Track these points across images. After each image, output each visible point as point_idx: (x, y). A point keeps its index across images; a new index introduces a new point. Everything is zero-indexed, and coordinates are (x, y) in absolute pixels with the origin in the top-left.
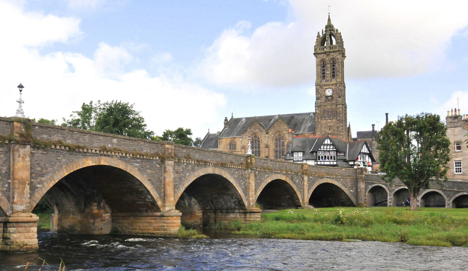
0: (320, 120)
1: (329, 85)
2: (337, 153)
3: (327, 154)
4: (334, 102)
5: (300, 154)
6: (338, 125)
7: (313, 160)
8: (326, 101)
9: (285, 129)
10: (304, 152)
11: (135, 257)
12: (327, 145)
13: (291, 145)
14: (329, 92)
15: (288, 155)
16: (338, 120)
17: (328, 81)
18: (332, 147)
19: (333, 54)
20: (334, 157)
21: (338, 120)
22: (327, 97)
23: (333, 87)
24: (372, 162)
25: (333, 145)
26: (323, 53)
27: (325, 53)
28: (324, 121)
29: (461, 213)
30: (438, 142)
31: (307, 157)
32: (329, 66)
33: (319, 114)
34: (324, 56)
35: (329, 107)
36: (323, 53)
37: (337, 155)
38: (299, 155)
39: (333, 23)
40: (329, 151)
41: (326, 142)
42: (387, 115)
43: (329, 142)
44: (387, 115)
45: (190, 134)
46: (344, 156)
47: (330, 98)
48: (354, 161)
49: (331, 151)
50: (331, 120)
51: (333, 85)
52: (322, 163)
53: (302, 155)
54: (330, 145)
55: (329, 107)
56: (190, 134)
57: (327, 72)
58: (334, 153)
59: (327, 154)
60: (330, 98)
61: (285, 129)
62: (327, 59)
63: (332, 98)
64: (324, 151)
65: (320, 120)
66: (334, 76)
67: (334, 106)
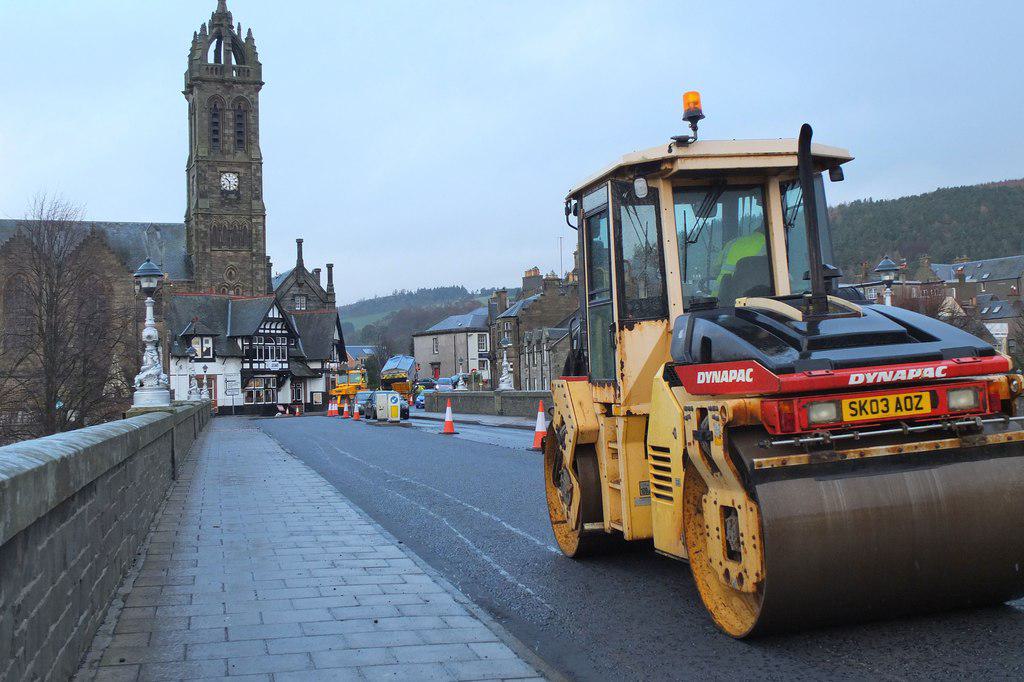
0: (208, 250)
1: (230, 164)
4: (244, 207)
5: (207, 342)
8: (223, 204)
11: (198, 182)
12: (273, 320)
14: (230, 181)
16: (253, 255)
17: (229, 153)
18: (279, 327)
19: (240, 87)
21: (253, 255)
22: (225, 193)
23: (242, 170)
26: (216, 81)
27: (222, 82)
29: (474, 431)
31: (225, 351)
32: (230, 115)
34: (219, 90)
35: (230, 218)
36: (216, 81)
39: (230, 7)
41: (270, 316)
42: (300, 242)
43: (276, 316)
44: (300, 242)
45: (837, 176)
47: (233, 196)
49: (280, 335)
50: (235, 251)
51: (240, 165)
52: (262, 366)
53: (210, 345)
54: (277, 321)
55: (230, 218)
56: (837, 176)
57: (226, 131)
60: (233, 196)
62: (226, 97)
63: (239, 198)
66: (240, 141)
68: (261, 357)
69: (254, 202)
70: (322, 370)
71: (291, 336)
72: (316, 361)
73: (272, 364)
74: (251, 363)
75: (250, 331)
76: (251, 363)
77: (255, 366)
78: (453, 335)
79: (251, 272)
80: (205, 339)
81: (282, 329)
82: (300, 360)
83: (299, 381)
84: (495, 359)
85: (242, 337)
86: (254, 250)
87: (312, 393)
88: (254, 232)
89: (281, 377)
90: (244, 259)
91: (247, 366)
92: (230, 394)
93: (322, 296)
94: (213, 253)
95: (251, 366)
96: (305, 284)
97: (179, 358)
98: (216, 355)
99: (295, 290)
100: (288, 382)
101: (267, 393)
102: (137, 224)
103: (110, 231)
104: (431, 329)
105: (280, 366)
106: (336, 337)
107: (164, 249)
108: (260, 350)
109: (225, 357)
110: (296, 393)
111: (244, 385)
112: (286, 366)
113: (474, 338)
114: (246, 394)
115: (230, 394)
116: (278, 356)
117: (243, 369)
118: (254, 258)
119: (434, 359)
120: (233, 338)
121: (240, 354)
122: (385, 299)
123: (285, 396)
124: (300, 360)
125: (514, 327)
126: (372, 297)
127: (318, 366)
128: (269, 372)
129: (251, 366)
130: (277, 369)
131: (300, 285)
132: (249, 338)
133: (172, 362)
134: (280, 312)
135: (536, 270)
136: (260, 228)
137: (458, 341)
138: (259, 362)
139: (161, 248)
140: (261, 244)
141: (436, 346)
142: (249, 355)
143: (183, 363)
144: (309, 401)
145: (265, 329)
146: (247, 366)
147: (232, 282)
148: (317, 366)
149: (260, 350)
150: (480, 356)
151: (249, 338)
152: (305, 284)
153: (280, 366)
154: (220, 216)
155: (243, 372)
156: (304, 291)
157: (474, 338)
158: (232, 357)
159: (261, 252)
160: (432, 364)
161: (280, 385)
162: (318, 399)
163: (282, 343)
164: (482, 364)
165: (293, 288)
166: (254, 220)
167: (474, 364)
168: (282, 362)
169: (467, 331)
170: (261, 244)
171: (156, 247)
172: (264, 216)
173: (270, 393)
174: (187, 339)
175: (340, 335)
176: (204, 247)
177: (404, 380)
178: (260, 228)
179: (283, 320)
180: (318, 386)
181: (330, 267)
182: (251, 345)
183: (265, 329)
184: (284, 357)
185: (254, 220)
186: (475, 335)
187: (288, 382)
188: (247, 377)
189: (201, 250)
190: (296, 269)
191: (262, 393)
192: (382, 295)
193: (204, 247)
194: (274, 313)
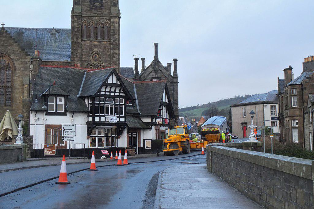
0: (80, 40)
2: (125, 102)
3: (110, 104)
4: (105, 12)
5: (60, 100)
6: (112, 52)
7: (85, 112)
8: (91, 9)
9: (13, 52)
10: (66, 97)
12: (112, 85)
13: (38, 81)
15: (36, 101)
16: (111, 44)
18: (118, 90)
20: (121, 109)
21: (111, 44)
24: (170, 118)
25: (120, 85)
28: (87, 43)
30: (84, 103)
31: (74, 107)
33: (78, 29)
37: (125, 105)
38: (59, 103)
40: (114, 97)
41: (110, 81)
42: (156, 45)
43: (115, 82)
44: (156, 45)
46: (133, 106)
48: (152, 117)
50: (99, 42)
52: (103, 119)
53: (63, 103)
54: (116, 86)
55: (96, 19)
58: (121, 101)
59: (110, 104)
61: (13, 52)
64: (105, 96)
65: (80, 40)
67: (105, 20)
68: (102, 113)
69: (113, 8)
70: (152, 124)
71: (128, 98)
72: (147, 117)
73: (113, 119)
74: (94, 117)
75: (92, 93)
76: (94, 117)
77: (97, 119)
78: (254, 106)
79: (110, 55)
80: (58, 98)
81: (120, 93)
82: (136, 116)
83: (134, 132)
84: (283, 118)
85: (88, 97)
86: (112, 41)
87: (144, 140)
88: (112, 28)
89: (119, 128)
90: (105, 47)
91: (91, 119)
92: (79, 139)
93: (170, 78)
94: (83, 43)
95: (93, 119)
96: (159, 71)
97: (36, 111)
98: (70, 110)
99: (153, 75)
100: (125, 132)
101: (107, 140)
102: (46, 29)
103: (26, 33)
104: (242, 103)
105: (118, 120)
106: (165, 99)
107: (57, 44)
108: (102, 108)
109: (73, 112)
110: (132, 141)
111: (89, 133)
112: (123, 120)
113: (268, 108)
114: (91, 140)
115: (79, 139)
116: (112, 113)
117: (88, 121)
118: (112, 46)
119: (243, 120)
120: (82, 98)
121: (86, 110)
122: (231, 99)
123: (123, 142)
124: (136, 116)
125: (299, 92)
126: (226, 99)
127: (148, 120)
128: (108, 124)
129: (93, 119)
130: (115, 122)
131: (156, 72)
132: (92, 98)
133: (32, 115)
134: (118, 78)
135: (303, 63)
136: (116, 25)
137: (258, 110)
138: (100, 116)
139: (55, 42)
140: (117, 36)
141: (244, 113)
142: (92, 111)
143: (40, 115)
144: (142, 146)
145: (105, 92)
146: (91, 119)
147: (97, 63)
148: (148, 120)
149: (102, 108)
150: (272, 119)
151: (92, 98)
152: (159, 71)
153: (118, 120)
154: (89, 17)
155: (88, 123)
156: (159, 75)
157: (268, 108)
158: (79, 112)
159: (117, 42)
160: (242, 124)
161: (119, 134)
162: (149, 145)
163: (120, 103)
164: (273, 124)
165: (151, 74)
166: (112, 20)
167: (268, 124)
168: (120, 117)
169: (264, 103)
170: (117, 36)
171: (53, 42)
172: (119, 18)
173: (110, 139)
174: (45, 98)
175: (169, 98)
176: (77, 39)
177: (217, 132)
178: (116, 25)
179: (120, 85)
180: (150, 135)
181: (175, 61)
182: (93, 103)
183: (110, 92)
184: (121, 113)
185: (112, 20)
186: (269, 106)
187: (125, 132)
188: (91, 127)
189: (75, 40)
190: (153, 62)
191: (103, 139)
192: (230, 97)
193: (77, 39)
194: (113, 80)
